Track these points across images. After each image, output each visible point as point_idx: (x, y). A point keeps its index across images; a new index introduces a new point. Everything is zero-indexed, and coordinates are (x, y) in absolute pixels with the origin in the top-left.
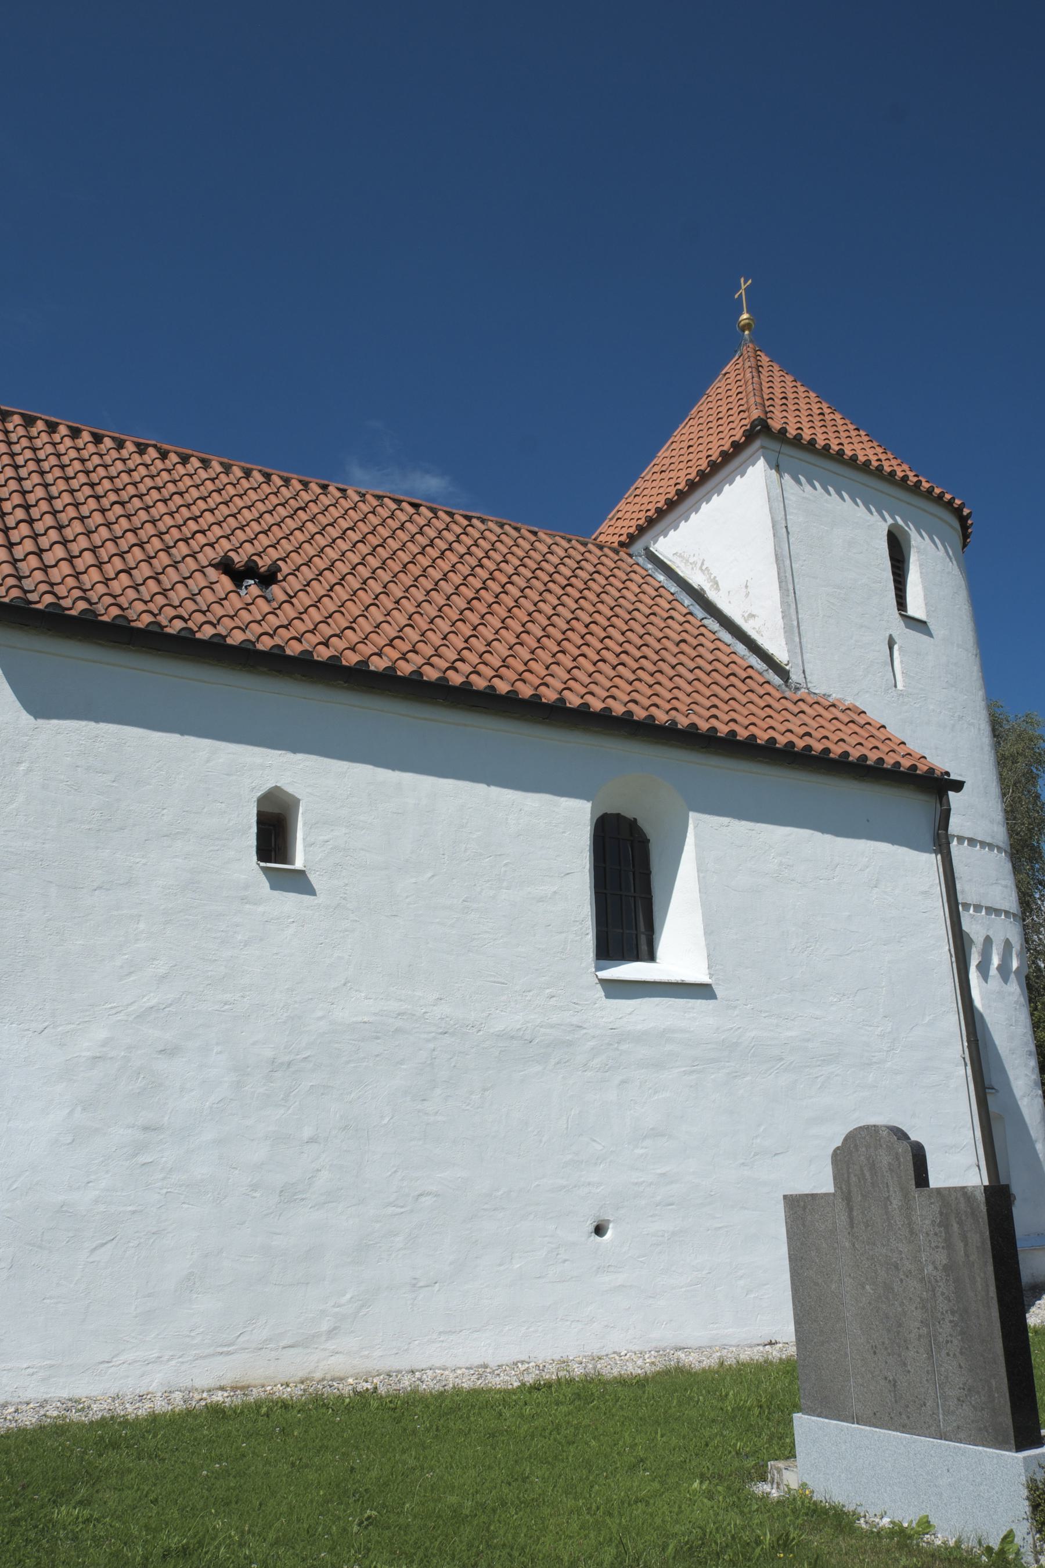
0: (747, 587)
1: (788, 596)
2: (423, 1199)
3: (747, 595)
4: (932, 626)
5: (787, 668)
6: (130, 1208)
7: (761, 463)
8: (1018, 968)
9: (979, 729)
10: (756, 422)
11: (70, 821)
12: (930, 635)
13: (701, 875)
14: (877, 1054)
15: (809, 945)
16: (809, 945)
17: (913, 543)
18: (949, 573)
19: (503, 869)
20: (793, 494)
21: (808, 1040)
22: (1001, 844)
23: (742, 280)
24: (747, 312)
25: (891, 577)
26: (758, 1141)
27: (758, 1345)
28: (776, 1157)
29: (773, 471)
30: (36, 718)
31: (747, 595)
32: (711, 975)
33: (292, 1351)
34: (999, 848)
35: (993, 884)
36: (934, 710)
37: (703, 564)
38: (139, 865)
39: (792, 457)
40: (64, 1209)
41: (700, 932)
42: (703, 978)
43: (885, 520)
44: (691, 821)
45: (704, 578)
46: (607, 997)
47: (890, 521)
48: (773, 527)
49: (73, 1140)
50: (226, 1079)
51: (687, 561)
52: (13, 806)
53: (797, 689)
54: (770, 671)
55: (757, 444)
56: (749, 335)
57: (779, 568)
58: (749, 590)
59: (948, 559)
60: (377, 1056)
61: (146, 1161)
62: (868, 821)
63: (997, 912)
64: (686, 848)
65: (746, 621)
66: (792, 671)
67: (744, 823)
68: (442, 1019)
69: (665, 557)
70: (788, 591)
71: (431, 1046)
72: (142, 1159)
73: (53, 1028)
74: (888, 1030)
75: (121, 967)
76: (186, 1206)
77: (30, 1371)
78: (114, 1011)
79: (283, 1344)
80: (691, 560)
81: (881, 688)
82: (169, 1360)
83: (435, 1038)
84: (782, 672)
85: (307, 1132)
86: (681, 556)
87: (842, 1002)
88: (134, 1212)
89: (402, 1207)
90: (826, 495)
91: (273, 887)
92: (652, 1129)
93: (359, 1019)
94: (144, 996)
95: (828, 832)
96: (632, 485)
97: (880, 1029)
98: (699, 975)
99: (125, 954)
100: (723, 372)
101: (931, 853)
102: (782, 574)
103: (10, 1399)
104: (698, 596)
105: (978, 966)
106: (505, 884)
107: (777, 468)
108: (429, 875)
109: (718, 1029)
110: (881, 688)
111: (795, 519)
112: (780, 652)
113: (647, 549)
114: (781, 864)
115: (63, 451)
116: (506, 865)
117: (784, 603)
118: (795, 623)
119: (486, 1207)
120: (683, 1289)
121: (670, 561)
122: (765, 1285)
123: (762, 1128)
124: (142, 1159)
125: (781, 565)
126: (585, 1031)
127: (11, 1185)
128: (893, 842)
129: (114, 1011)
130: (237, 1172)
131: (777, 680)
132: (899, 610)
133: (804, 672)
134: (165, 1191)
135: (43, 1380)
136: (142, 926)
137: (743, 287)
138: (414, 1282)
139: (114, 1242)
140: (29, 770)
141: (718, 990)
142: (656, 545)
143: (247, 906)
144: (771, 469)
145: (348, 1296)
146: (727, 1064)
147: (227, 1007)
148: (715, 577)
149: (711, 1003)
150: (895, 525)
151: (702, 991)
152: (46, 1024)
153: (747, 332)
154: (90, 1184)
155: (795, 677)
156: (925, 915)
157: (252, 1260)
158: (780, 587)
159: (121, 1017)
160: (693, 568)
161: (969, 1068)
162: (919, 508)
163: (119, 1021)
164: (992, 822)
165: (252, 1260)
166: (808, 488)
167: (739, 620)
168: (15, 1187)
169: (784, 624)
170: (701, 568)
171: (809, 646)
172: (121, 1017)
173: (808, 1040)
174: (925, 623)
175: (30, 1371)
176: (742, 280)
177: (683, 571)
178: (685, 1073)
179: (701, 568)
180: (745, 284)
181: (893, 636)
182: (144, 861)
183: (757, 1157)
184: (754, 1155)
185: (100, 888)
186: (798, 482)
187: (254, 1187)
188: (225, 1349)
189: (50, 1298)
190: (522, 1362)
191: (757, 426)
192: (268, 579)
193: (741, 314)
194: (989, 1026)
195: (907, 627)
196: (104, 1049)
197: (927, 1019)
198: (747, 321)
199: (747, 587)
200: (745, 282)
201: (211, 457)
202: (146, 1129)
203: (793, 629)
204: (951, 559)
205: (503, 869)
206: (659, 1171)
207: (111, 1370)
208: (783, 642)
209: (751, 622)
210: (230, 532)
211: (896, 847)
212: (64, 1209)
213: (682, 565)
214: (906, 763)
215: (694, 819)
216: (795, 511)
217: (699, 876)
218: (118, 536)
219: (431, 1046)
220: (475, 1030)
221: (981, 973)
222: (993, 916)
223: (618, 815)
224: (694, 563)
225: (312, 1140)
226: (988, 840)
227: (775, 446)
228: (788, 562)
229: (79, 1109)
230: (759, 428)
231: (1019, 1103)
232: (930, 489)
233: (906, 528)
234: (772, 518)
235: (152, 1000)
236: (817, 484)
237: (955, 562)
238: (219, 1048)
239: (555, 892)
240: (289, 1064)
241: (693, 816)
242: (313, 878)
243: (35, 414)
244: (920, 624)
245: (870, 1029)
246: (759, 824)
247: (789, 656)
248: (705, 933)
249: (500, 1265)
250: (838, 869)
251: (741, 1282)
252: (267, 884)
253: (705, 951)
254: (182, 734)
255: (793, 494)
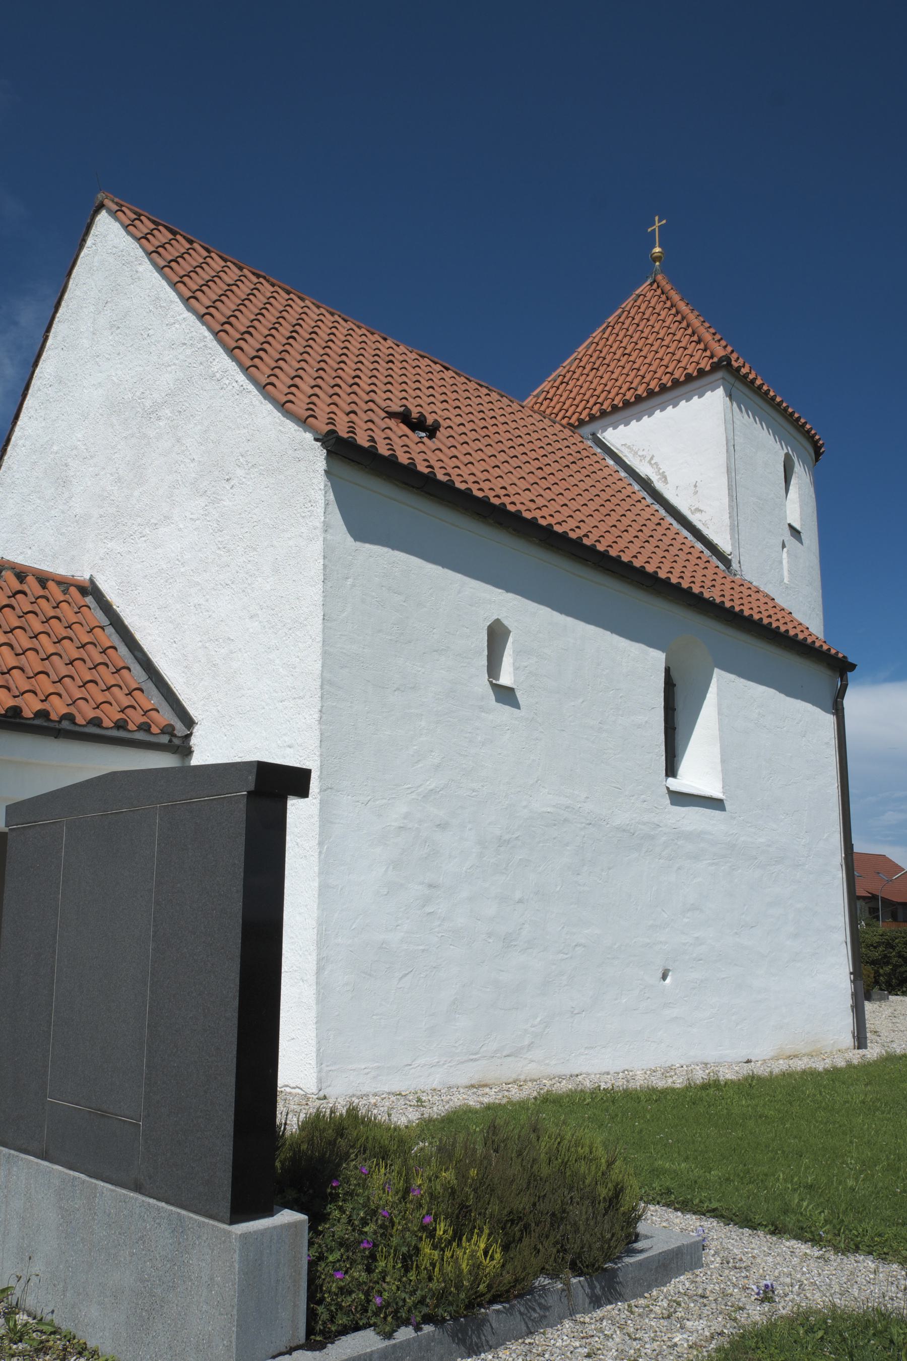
0: (695, 486)
2: (577, 949)
3: (696, 493)
5: (730, 557)
6: (421, 947)
7: (720, 391)
11: (380, 631)
19: (620, 701)
23: (657, 218)
24: (659, 247)
27: (741, 1062)
30: (356, 540)
31: (696, 493)
32: (724, 793)
33: (509, 1059)
37: (652, 458)
38: (420, 673)
40: (384, 946)
41: (718, 760)
42: (717, 793)
44: (714, 675)
45: (652, 470)
46: (672, 804)
47: (786, 451)
49: (388, 892)
50: (474, 850)
51: (636, 453)
52: (344, 615)
53: (735, 575)
54: (714, 557)
55: (719, 374)
56: (659, 266)
57: (728, 479)
58: (697, 489)
60: (554, 838)
61: (430, 911)
64: (708, 695)
65: (692, 513)
66: (733, 560)
67: (742, 680)
68: (588, 813)
69: (613, 446)
71: (583, 833)
72: (429, 909)
73: (374, 801)
75: (413, 756)
76: (452, 947)
77: (366, 1071)
78: (409, 791)
79: (505, 1053)
80: (640, 453)
82: (444, 1064)
83: (585, 827)
85: (518, 895)
86: (629, 447)
88: (423, 951)
89: (567, 954)
91: (498, 700)
92: (692, 904)
93: (545, 809)
94: (427, 780)
96: (554, 371)
98: (714, 790)
99: (415, 745)
100: (637, 292)
103: (355, 1092)
104: (646, 484)
106: (621, 712)
107: (730, 395)
108: (581, 700)
112: (724, 543)
113: (594, 434)
116: (621, 697)
117: (730, 506)
119: (609, 956)
121: (618, 449)
124: (429, 909)
126: (661, 829)
127: (351, 926)
128: (813, 705)
129: (409, 791)
130: (480, 922)
131: (722, 567)
133: (739, 562)
134: (441, 934)
135: (374, 1077)
136: (423, 723)
137: (657, 224)
138: (572, 1010)
139: (413, 973)
140: (353, 586)
141: (727, 804)
142: (605, 434)
143: (483, 714)
145: (539, 1019)
147: (474, 794)
148: (664, 472)
151: (715, 804)
152: (369, 797)
153: (657, 263)
154: (398, 927)
155: (735, 565)
157: (489, 990)
159: (414, 796)
160: (641, 460)
161: (844, 872)
163: (413, 799)
165: (489, 990)
167: (684, 509)
168: (353, 927)
170: (650, 462)
172: (414, 796)
175: (366, 1071)
176: (657, 218)
177: (630, 460)
179: (650, 462)
180: (659, 222)
182: (423, 670)
185: (398, 689)
187: (490, 935)
188: (474, 1057)
189: (377, 1015)
190: (627, 1070)
191: (723, 361)
192: (432, 431)
193: (654, 247)
195: (792, 535)
196: (405, 821)
197: (826, 835)
198: (659, 254)
199: (695, 486)
200: (659, 221)
201: (307, 297)
202: (430, 886)
203: (734, 528)
205: (620, 701)
206: (696, 935)
207: (412, 1071)
208: (729, 537)
209: (698, 515)
212: (384, 946)
213: (630, 456)
214: (809, 640)
219: (583, 833)
220: (605, 823)
224: (644, 457)
225: (520, 901)
227: (732, 380)
229: (391, 867)
230: (725, 363)
235: (432, 784)
238: (469, 826)
239: (646, 722)
240: (509, 841)
241: (717, 672)
242: (518, 694)
243: (178, 230)
249: (616, 999)
252: (494, 698)
254: (443, 567)
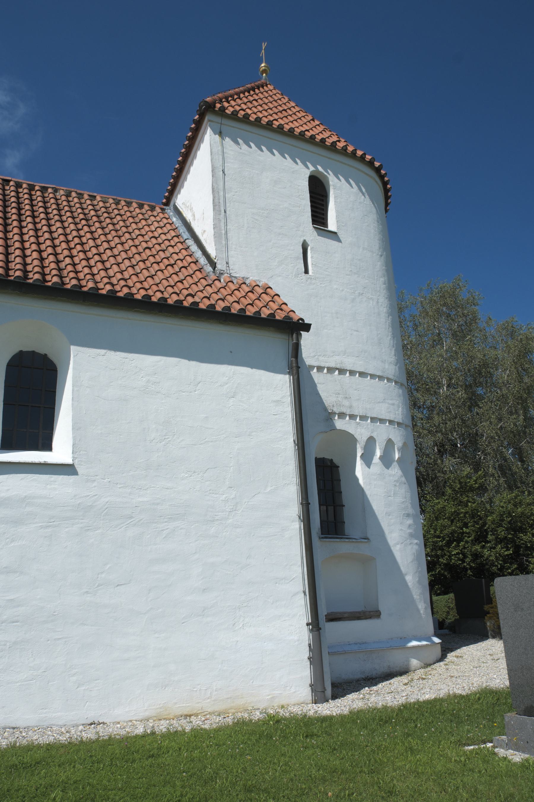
1: (220, 214)
4: (341, 235)
5: (216, 261)
8: (399, 458)
9: (378, 302)
10: (202, 104)
12: (339, 241)
13: (75, 389)
14: (220, 513)
15: (167, 437)
16: (167, 437)
17: (331, 183)
18: (360, 203)
20: (232, 150)
21: (158, 504)
22: (391, 377)
25: (309, 204)
26: (103, 575)
28: (118, 587)
29: (217, 136)
34: (389, 380)
35: (379, 402)
36: (337, 289)
39: (233, 127)
42: (69, 461)
43: (308, 168)
47: (312, 168)
48: (212, 171)
59: (361, 194)
62: (231, 352)
63: (382, 421)
70: (220, 211)
74: (232, 497)
81: (292, 273)
84: (213, 265)
87: (192, 478)
90: (259, 151)
92: (5, 568)
95: (193, 360)
97: (224, 496)
98: (68, 460)
101: (285, 374)
102: (216, 201)
105: (362, 456)
107: (220, 134)
109: (75, 496)
110: (292, 273)
111: (231, 167)
112: (212, 251)
114: (148, 381)
115: (111, 239)
118: (223, 232)
120: (18, 684)
122: (96, 680)
123: (108, 566)
125: (217, 195)
132: (313, 224)
144: (215, 134)
146: (81, 521)
149: (72, 478)
150: (317, 171)
153: (264, 75)
155: (220, 266)
156: (275, 416)
158: (214, 209)
162: (338, 161)
164: (383, 362)
166: (244, 147)
169: (215, 232)
171: (234, 246)
173: (158, 504)
174: (335, 233)
178: (41, 527)
181: (307, 241)
183: (100, 587)
184: (98, 586)
186: (237, 143)
193: (262, 64)
194: (369, 497)
197: (269, 489)
204: (363, 194)
206: (8, 598)
210: (192, 273)
211: (254, 370)
213: (184, 209)
215: (74, 350)
216: (232, 161)
217: (73, 390)
218: (143, 280)
221: (364, 461)
222: (378, 424)
223: (33, 352)
226: (379, 373)
227: (218, 119)
228: (221, 193)
231: (392, 548)
232: (344, 148)
233: (325, 173)
234: (212, 166)
236: (298, 161)
237: (367, 196)
244: (332, 234)
245: (215, 496)
246: (132, 354)
247: (216, 253)
248: (73, 429)
250: (200, 385)
251: (74, 678)
253: (72, 441)
255: (232, 150)
